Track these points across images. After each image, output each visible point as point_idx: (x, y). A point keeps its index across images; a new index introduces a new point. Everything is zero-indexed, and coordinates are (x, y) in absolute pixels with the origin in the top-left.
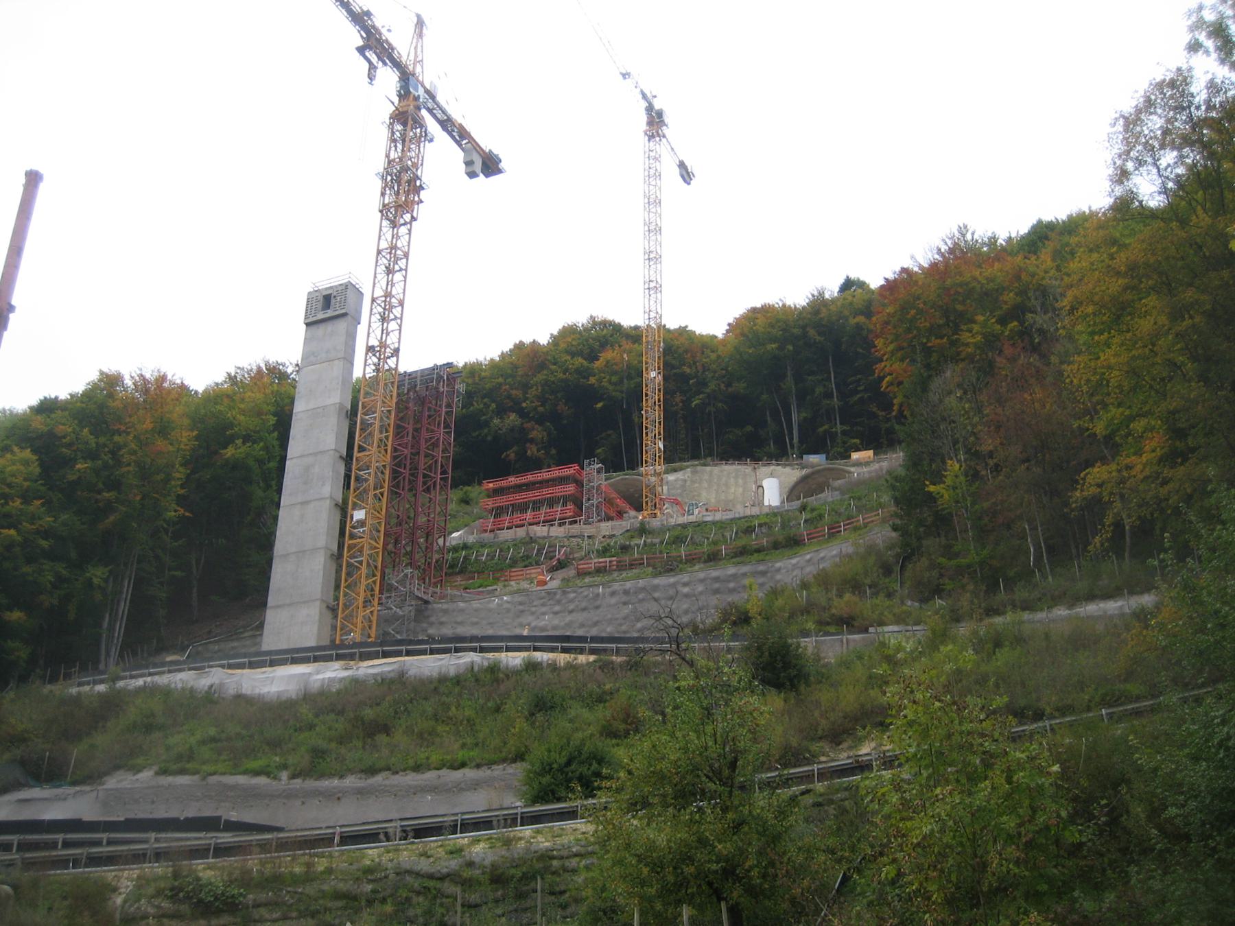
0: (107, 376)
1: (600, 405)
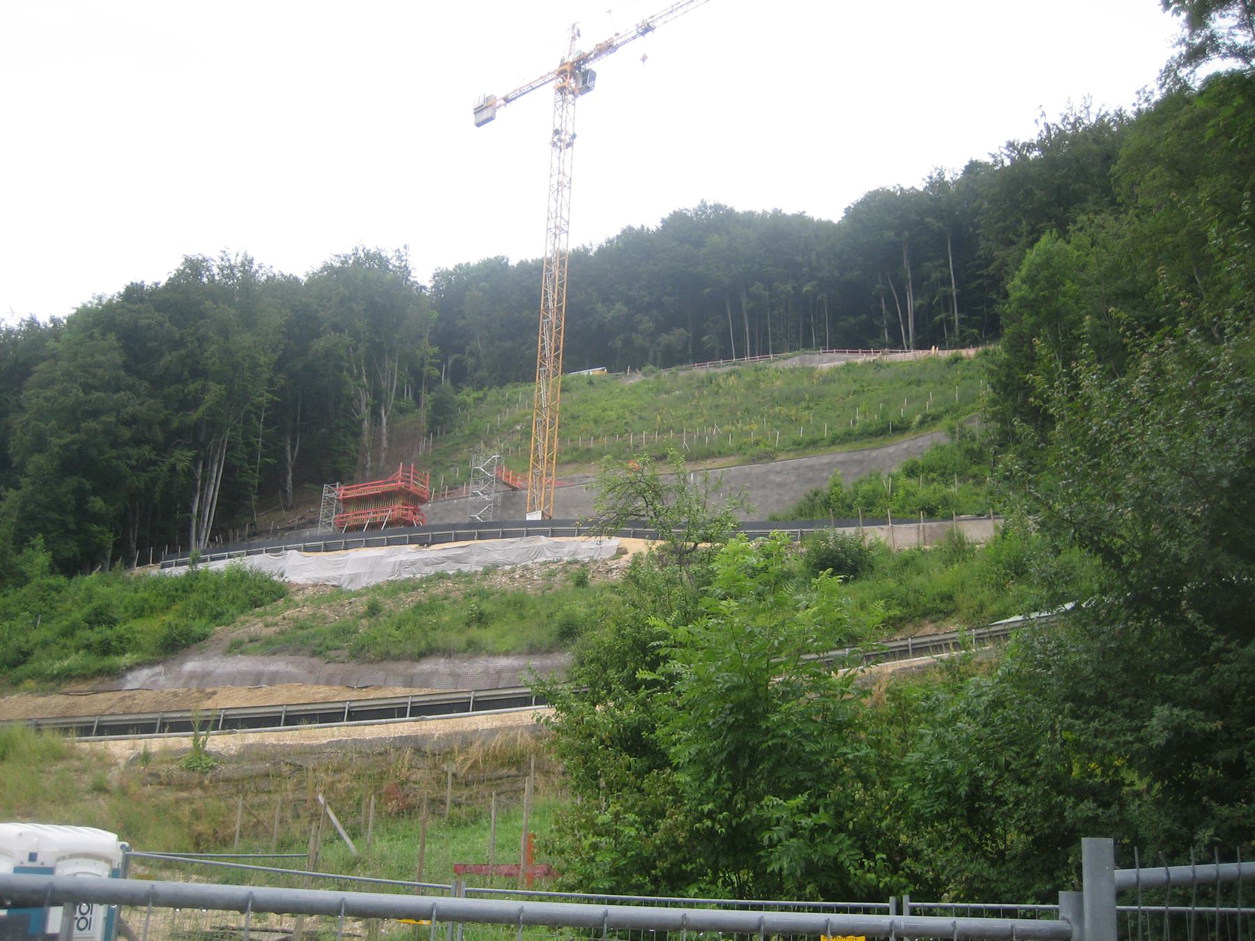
0: (191, 261)
1: (707, 291)
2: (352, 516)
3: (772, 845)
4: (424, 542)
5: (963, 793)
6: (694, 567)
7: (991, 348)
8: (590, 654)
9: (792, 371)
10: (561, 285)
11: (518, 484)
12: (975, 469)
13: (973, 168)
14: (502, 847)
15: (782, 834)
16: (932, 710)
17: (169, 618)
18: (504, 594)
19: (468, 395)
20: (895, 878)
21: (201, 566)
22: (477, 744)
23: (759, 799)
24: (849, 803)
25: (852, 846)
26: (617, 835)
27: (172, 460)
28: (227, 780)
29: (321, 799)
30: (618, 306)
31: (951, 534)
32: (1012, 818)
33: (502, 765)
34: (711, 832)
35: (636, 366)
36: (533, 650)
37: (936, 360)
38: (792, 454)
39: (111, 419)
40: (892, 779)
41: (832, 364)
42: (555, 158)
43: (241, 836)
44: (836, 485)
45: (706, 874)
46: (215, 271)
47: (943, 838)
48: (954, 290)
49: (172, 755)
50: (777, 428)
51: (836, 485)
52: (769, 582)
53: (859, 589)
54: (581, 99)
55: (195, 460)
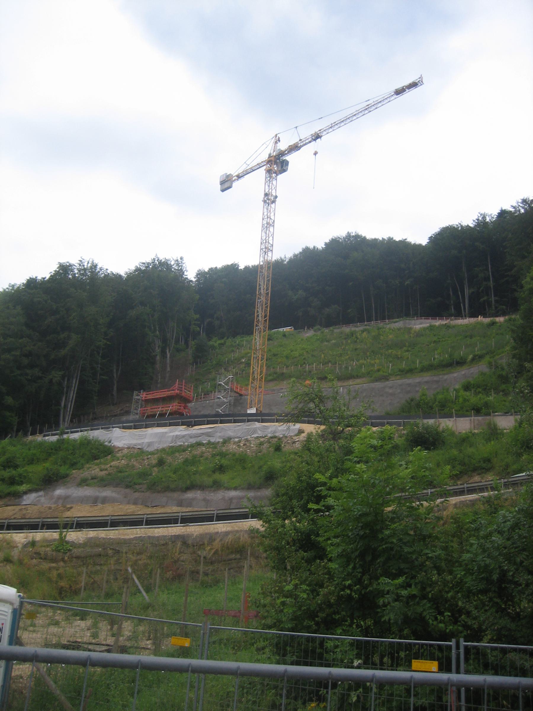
0: (63, 266)
1: (351, 284)
2: (149, 409)
3: (385, 605)
4: (189, 425)
5: (495, 578)
6: (342, 442)
7: (513, 317)
8: (283, 491)
9: (399, 329)
10: (268, 281)
11: (243, 392)
12: (503, 386)
13: (503, 213)
14: (231, 600)
15: (390, 599)
16: (477, 529)
17: (47, 465)
18: (234, 455)
19: (215, 342)
20: (456, 627)
21: (65, 436)
22: (218, 540)
23: (377, 578)
24: (430, 583)
25: (430, 608)
26: (296, 597)
27: (51, 377)
28: (78, 558)
29: (130, 570)
30: (300, 292)
31: (489, 424)
32: (524, 593)
33: (232, 553)
34: (350, 596)
35: (310, 326)
36: (250, 487)
37: (481, 324)
38: (398, 377)
39: (18, 353)
40: (454, 569)
41: (421, 326)
42: (265, 210)
43: (85, 589)
44: (423, 395)
45: (347, 621)
46: (76, 271)
47: (484, 605)
48: (491, 284)
49: (47, 543)
50: (390, 362)
51: (423, 395)
52: (386, 451)
53: (437, 455)
54: (280, 177)
55: (63, 377)
